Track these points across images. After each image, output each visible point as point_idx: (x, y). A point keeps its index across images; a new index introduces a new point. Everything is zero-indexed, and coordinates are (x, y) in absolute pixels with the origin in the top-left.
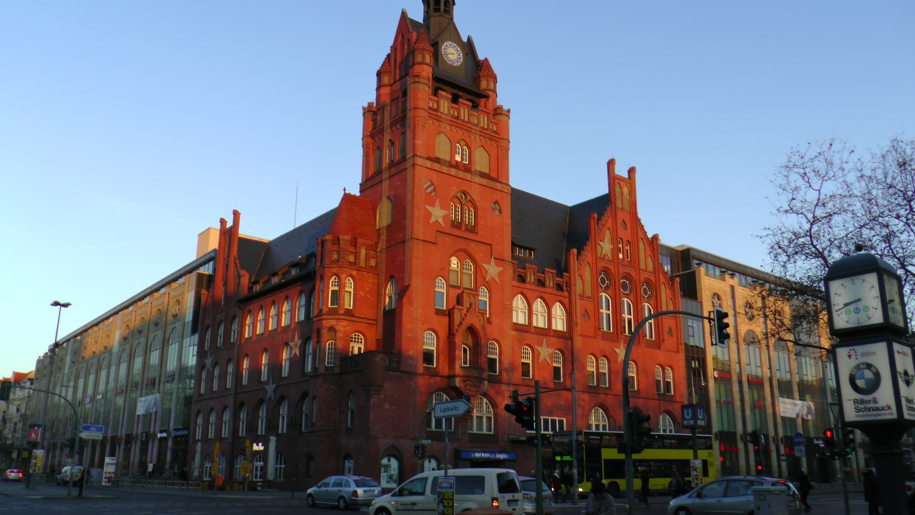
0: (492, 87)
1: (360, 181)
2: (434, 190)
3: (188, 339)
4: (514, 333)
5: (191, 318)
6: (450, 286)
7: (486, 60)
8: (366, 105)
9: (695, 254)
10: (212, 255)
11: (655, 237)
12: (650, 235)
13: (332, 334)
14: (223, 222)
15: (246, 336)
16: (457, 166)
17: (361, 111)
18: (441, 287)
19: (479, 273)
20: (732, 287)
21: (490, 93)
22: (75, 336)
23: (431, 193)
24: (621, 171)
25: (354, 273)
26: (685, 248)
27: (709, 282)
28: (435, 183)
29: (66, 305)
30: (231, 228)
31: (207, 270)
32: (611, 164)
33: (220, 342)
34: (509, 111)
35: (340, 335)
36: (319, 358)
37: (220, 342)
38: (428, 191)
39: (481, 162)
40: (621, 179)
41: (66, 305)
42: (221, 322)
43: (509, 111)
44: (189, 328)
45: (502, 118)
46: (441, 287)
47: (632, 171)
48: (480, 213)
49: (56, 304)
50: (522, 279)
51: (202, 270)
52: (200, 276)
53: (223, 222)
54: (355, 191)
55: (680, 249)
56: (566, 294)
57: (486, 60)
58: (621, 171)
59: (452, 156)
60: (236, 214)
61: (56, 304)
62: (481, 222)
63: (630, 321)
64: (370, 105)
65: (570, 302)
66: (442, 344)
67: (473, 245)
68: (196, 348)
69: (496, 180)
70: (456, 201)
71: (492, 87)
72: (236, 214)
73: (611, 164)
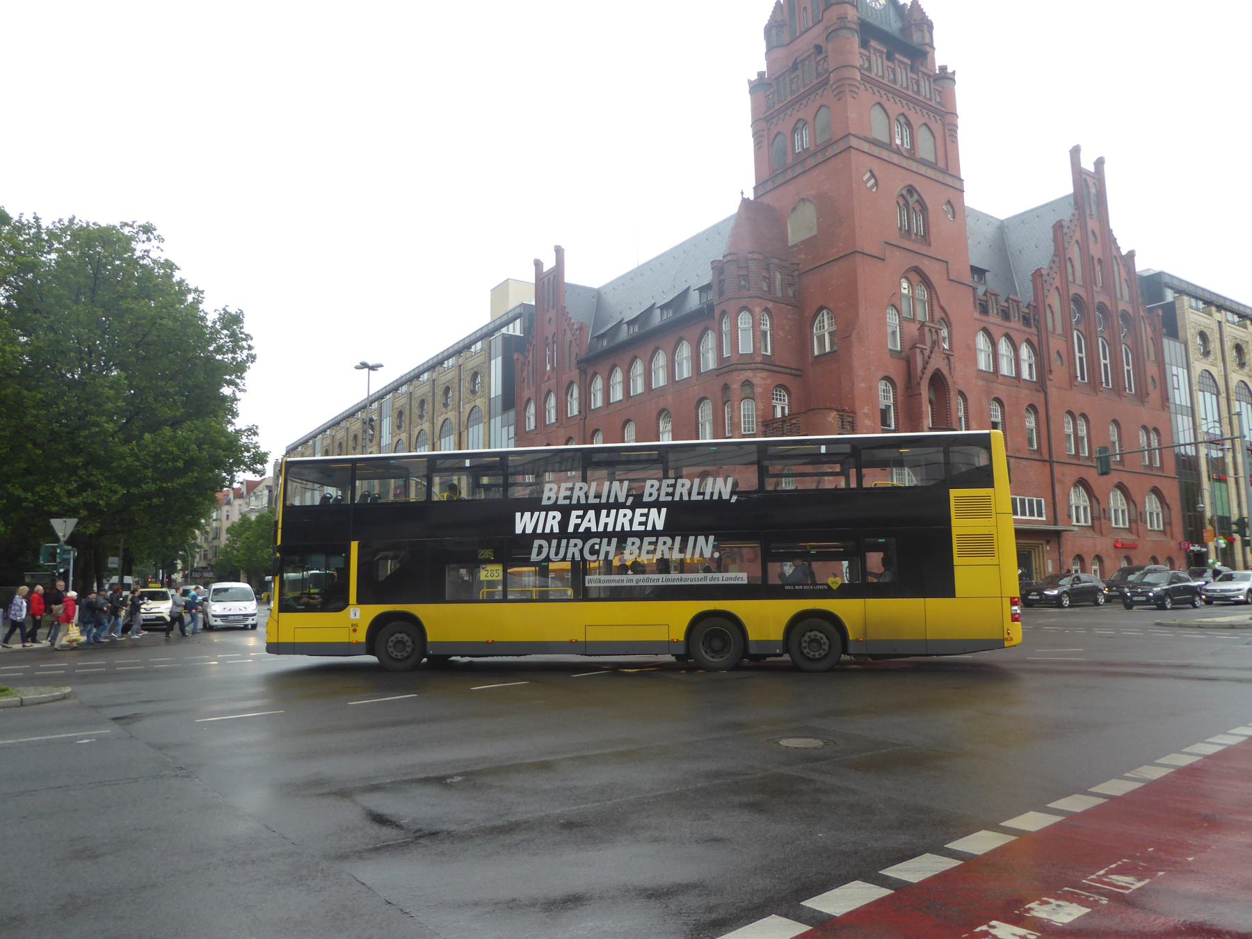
0: (927, 40)
1: (754, 184)
2: (876, 184)
3: (499, 419)
4: (981, 383)
5: (499, 392)
6: (902, 319)
7: (232, 321)
8: (754, 77)
9: (1167, 279)
10: (518, 311)
11: (1131, 254)
12: (1124, 252)
13: (748, 390)
14: (538, 264)
15: (816, 353)
16: (898, 151)
17: (747, 88)
18: (892, 319)
19: (935, 302)
20: (1220, 322)
21: (928, 49)
22: (325, 431)
23: (872, 187)
24: (1088, 164)
25: (770, 305)
26: (1151, 273)
27: (1193, 318)
28: (876, 174)
29: (373, 368)
30: (551, 271)
31: (515, 329)
32: (1075, 152)
33: (552, 417)
34: (954, 73)
35: (758, 390)
36: (732, 424)
37: (552, 417)
38: (869, 184)
39: (925, 149)
40: (1088, 173)
41: (373, 368)
42: (549, 392)
43: (954, 73)
44: (499, 405)
45: (947, 82)
46: (892, 319)
47: (1100, 163)
48: (932, 218)
49: (364, 365)
50: (984, 310)
51: (504, 330)
52: (507, 340)
53: (538, 264)
54: (750, 195)
55: (1145, 274)
56: (1034, 330)
57: (232, 321)
58: (1088, 164)
59: (891, 138)
60: (559, 251)
61: (364, 365)
62: (933, 230)
63: (1105, 365)
64: (761, 74)
65: (1040, 341)
66: (900, 398)
67: (926, 261)
68: (512, 429)
69: (945, 171)
70: (902, 202)
71: (927, 40)
72: (559, 251)
73: (1075, 152)
